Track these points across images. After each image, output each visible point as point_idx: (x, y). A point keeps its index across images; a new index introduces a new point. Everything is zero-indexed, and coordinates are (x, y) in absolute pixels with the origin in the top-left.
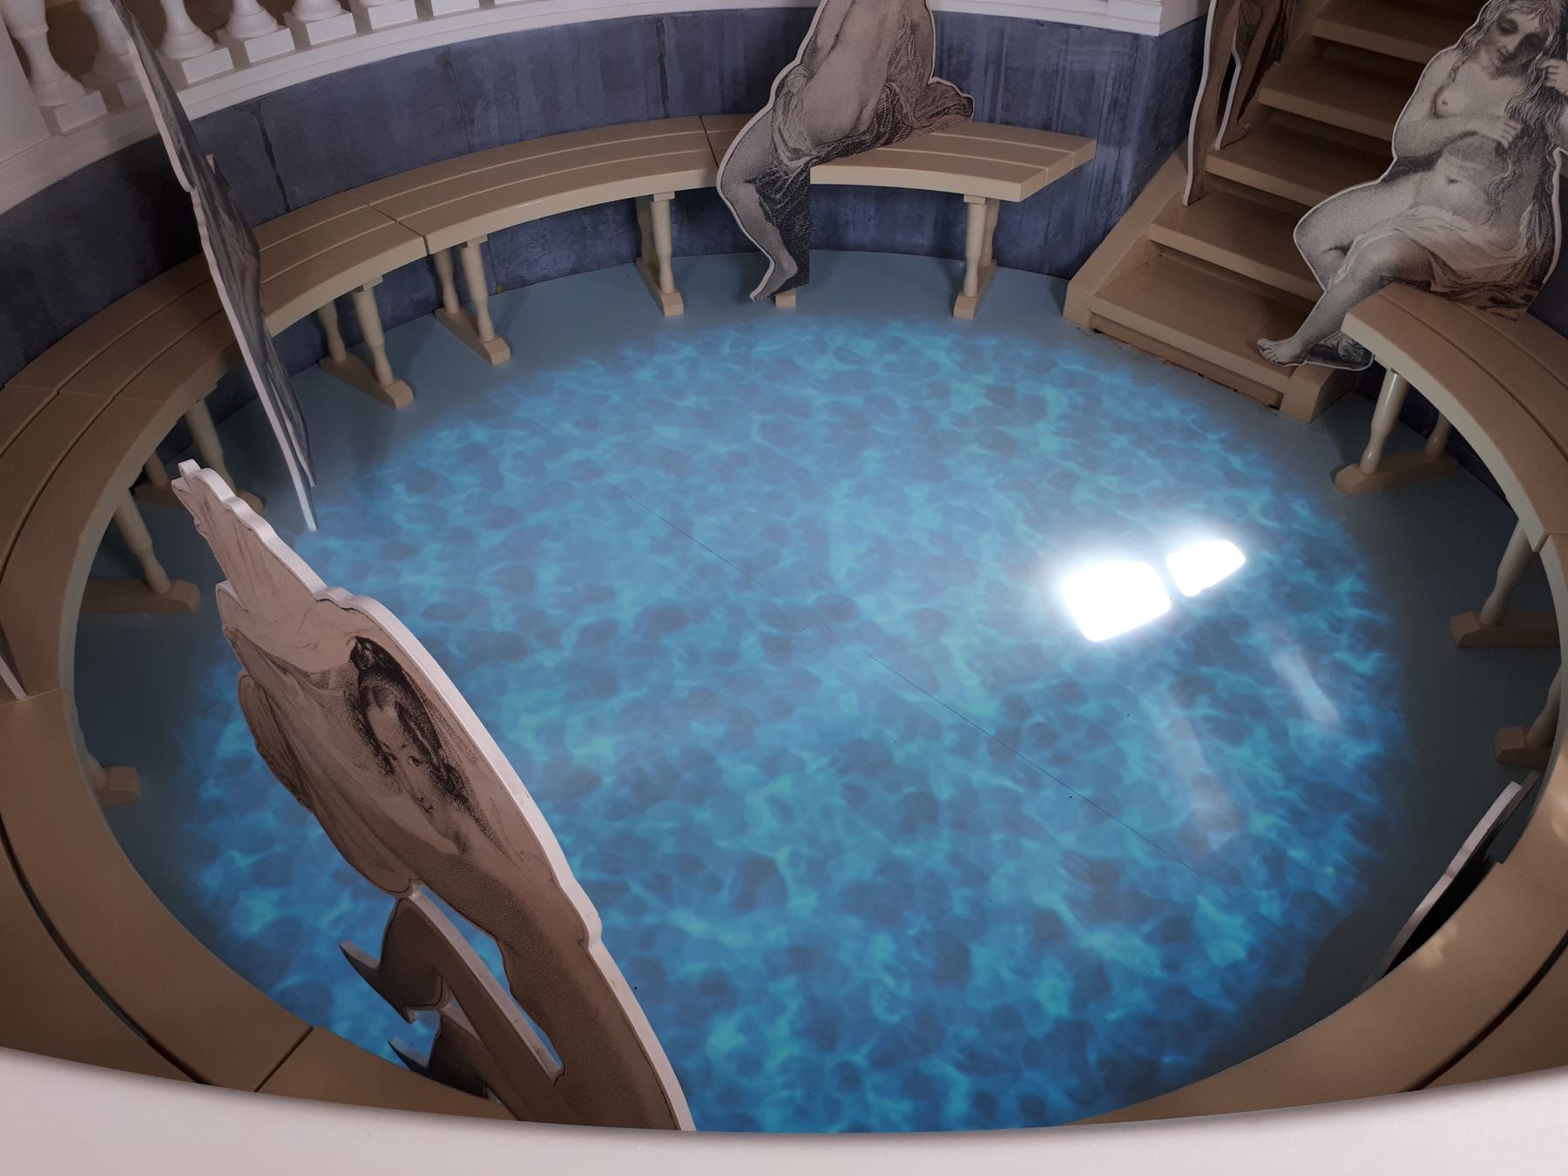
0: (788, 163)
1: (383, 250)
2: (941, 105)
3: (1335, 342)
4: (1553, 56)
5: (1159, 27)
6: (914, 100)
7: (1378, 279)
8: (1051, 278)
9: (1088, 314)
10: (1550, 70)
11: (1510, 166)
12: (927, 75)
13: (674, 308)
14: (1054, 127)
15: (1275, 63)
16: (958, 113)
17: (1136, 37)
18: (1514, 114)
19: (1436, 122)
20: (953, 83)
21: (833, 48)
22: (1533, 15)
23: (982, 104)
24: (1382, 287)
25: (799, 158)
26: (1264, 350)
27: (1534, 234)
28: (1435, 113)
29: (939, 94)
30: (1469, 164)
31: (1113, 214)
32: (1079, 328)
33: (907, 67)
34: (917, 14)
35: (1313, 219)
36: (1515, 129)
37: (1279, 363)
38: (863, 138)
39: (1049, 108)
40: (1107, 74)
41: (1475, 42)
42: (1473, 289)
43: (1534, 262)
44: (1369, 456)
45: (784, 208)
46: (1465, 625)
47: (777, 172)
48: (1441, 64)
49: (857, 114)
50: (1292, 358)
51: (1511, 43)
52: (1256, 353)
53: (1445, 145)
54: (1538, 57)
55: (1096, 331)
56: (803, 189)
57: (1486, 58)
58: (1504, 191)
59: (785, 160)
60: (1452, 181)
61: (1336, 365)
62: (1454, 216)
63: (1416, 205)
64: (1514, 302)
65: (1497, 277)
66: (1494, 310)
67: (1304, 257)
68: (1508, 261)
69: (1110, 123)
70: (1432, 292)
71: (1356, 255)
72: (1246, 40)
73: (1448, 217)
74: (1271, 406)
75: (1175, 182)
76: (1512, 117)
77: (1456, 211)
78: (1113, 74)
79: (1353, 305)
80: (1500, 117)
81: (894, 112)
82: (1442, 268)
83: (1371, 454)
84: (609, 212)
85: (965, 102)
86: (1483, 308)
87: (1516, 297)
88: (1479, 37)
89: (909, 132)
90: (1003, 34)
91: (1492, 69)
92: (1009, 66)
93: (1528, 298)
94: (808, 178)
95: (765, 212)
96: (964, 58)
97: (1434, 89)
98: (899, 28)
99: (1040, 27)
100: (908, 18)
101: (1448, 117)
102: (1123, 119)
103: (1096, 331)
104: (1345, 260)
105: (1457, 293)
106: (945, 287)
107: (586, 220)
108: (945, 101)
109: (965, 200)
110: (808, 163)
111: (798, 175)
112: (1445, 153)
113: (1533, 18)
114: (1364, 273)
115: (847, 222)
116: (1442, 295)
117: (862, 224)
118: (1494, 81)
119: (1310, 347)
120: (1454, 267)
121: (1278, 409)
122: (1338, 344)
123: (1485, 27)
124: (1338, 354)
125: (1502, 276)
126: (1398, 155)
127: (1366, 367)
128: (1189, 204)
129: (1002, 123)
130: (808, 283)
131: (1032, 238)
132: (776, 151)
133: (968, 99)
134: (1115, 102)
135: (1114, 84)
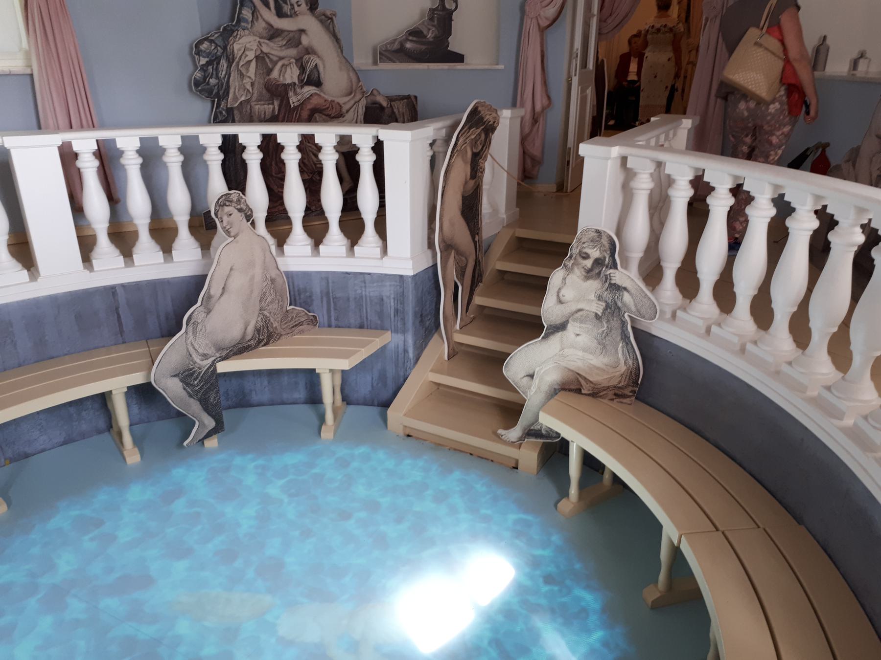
0: (201, 363)
2: (297, 321)
3: (539, 427)
4: (611, 268)
5: (412, 271)
6: (279, 319)
7: (553, 390)
8: (379, 408)
9: (402, 427)
10: (612, 275)
11: (605, 324)
12: (285, 306)
13: (133, 457)
14: (366, 326)
15: (480, 284)
16: (308, 324)
17: (401, 277)
18: (600, 298)
20: (304, 308)
21: (222, 295)
22: (595, 249)
23: (322, 317)
24: (556, 395)
25: (207, 359)
26: (502, 436)
27: (626, 358)
28: (560, 302)
30: (584, 325)
31: (407, 369)
33: (272, 302)
34: (273, 273)
35: (511, 362)
36: (602, 305)
37: (512, 442)
38: (249, 343)
39: (361, 316)
40: (390, 296)
41: (570, 264)
42: (604, 390)
43: (631, 372)
44: (573, 492)
45: (201, 388)
46: (651, 594)
47: (193, 368)
48: (556, 277)
49: (243, 330)
50: (518, 438)
51: (589, 263)
52: (498, 438)
53: (570, 317)
54: (603, 269)
55: (409, 436)
56: (213, 378)
57: (578, 272)
58: (605, 337)
59: (198, 361)
60: (578, 335)
61: (543, 439)
62: (584, 353)
63: (563, 349)
64: (627, 395)
65: (614, 382)
66: (618, 400)
67: (511, 382)
70: (582, 394)
71: (538, 379)
72: (461, 273)
73: (580, 353)
74: (514, 468)
75: (438, 348)
76: (599, 300)
77: (584, 350)
78: (392, 296)
79: (542, 406)
80: (593, 300)
81: (268, 327)
82: (585, 380)
83: (573, 490)
84: (89, 403)
85: (312, 318)
86: (612, 400)
87: (627, 392)
88: (572, 262)
89: (280, 337)
90: (328, 281)
91: (583, 277)
92: (334, 296)
93: (633, 392)
94: (215, 369)
95: (188, 393)
96: (308, 294)
97: (556, 289)
98: (264, 282)
99: (349, 275)
100: (268, 276)
101: (567, 303)
102: (403, 319)
103: (409, 436)
105: (596, 393)
106: (316, 422)
107: (72, 410)
109: (317, 371)
110: (214, 361)
111: (208, 368)
112: (570, 321)
113: (596, 250)
114: (545, 388)
115: (251, 391)
116: (589, 395)
117: (261, 391)
118: (585, 283)
119: (527, 431)
120: (591, 380)
121: (517, 468)
122: (541, 428)
123: (574, 257)
124: (542, 434)
125: (617, 381)
126: (547, 325)
127: (559, 439)
128: (449, 359)
129: (336, 327)
130: (224, 431)
131: (364, 386)
132: (191, 356)
133: (314, 316)
134: (397, 311)
135: (394, 301)
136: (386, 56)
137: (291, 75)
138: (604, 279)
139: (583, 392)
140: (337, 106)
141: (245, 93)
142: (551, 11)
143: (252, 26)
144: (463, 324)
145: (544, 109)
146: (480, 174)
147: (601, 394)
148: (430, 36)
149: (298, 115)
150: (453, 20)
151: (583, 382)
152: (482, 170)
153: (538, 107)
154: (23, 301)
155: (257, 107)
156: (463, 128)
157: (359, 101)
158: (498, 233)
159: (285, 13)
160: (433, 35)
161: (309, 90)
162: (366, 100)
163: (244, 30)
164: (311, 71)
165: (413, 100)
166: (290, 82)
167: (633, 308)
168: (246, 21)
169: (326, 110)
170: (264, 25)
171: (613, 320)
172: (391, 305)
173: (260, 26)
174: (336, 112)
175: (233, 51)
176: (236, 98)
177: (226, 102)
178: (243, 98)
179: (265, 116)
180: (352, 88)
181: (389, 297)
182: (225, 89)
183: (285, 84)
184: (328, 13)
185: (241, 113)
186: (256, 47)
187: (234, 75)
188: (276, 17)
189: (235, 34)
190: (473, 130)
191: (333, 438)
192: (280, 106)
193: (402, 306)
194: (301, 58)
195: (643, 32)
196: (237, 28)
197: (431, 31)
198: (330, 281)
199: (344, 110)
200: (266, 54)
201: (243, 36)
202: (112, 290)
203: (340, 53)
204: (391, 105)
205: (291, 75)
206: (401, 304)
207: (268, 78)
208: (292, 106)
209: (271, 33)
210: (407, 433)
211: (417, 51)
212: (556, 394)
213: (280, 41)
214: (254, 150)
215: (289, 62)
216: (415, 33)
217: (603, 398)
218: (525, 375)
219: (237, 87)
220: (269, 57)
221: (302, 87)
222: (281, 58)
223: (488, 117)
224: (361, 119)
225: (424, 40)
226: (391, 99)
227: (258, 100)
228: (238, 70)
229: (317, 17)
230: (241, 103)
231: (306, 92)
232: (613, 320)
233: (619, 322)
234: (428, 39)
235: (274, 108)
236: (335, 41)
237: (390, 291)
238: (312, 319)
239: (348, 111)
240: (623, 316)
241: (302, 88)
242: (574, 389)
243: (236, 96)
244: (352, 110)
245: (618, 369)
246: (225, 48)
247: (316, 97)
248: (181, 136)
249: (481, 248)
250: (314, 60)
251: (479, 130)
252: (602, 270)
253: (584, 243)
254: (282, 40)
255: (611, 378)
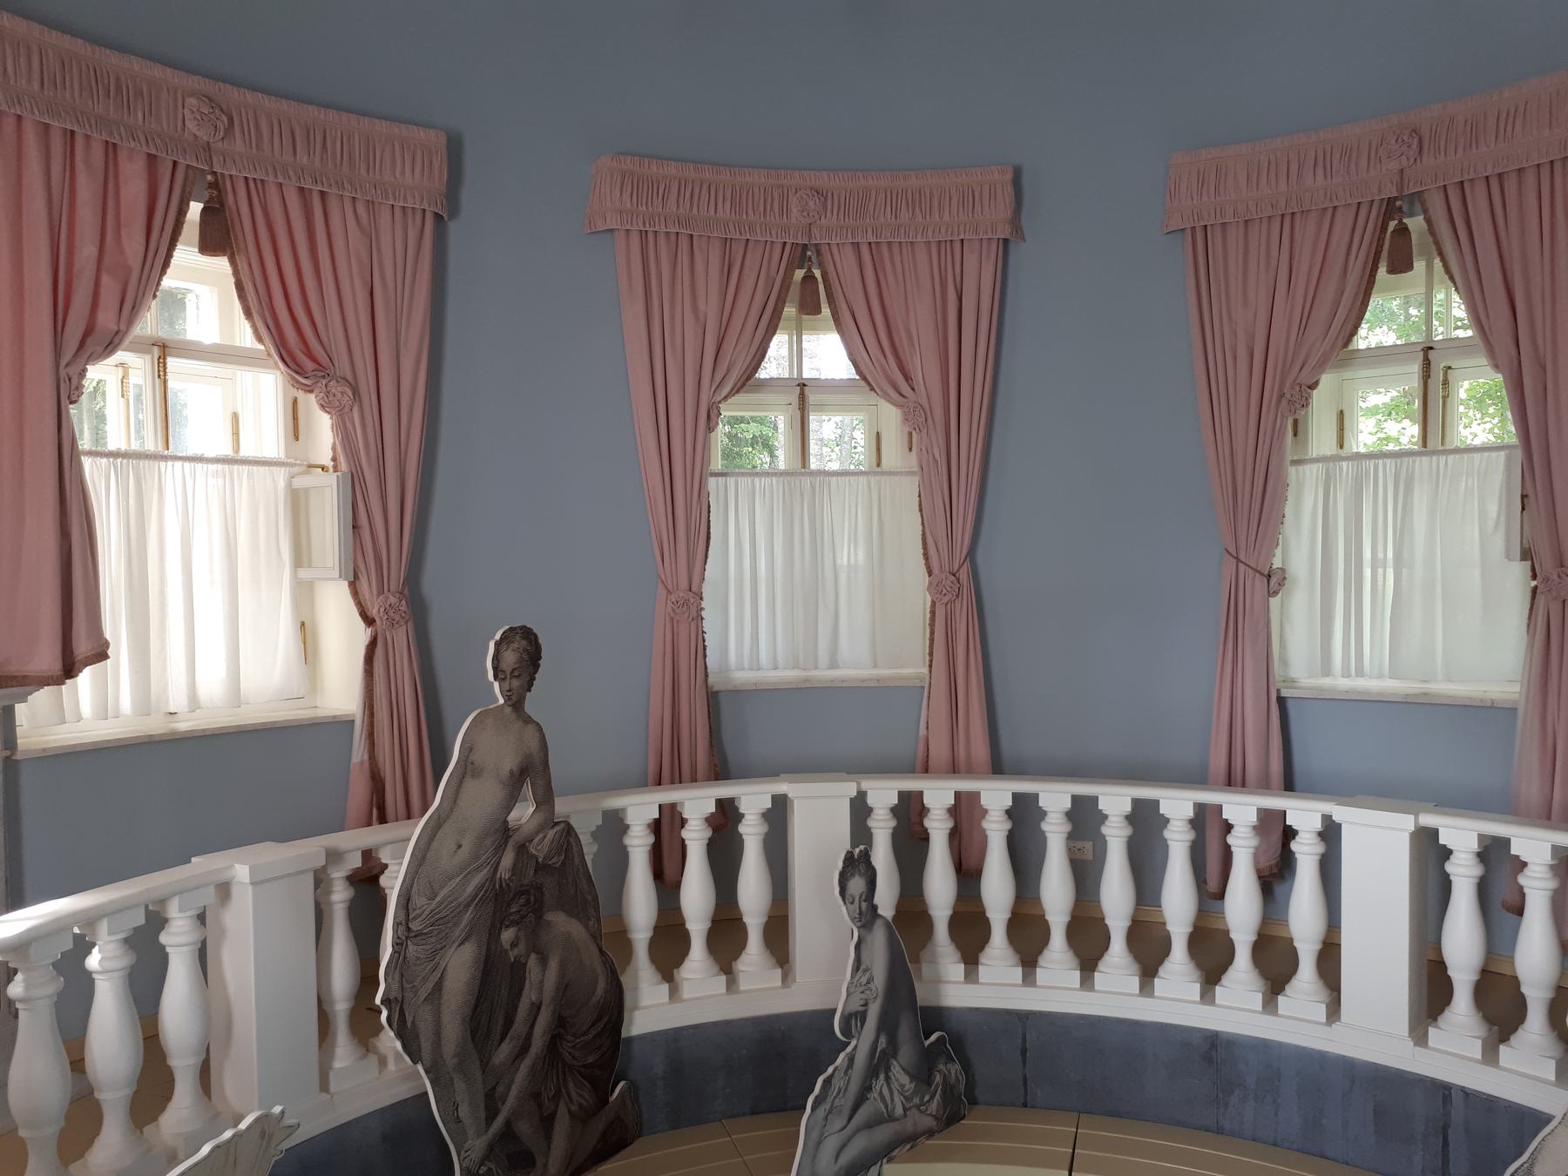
154: (1304, 1049)
202: (1443, 1092)
248: (1013, 793)
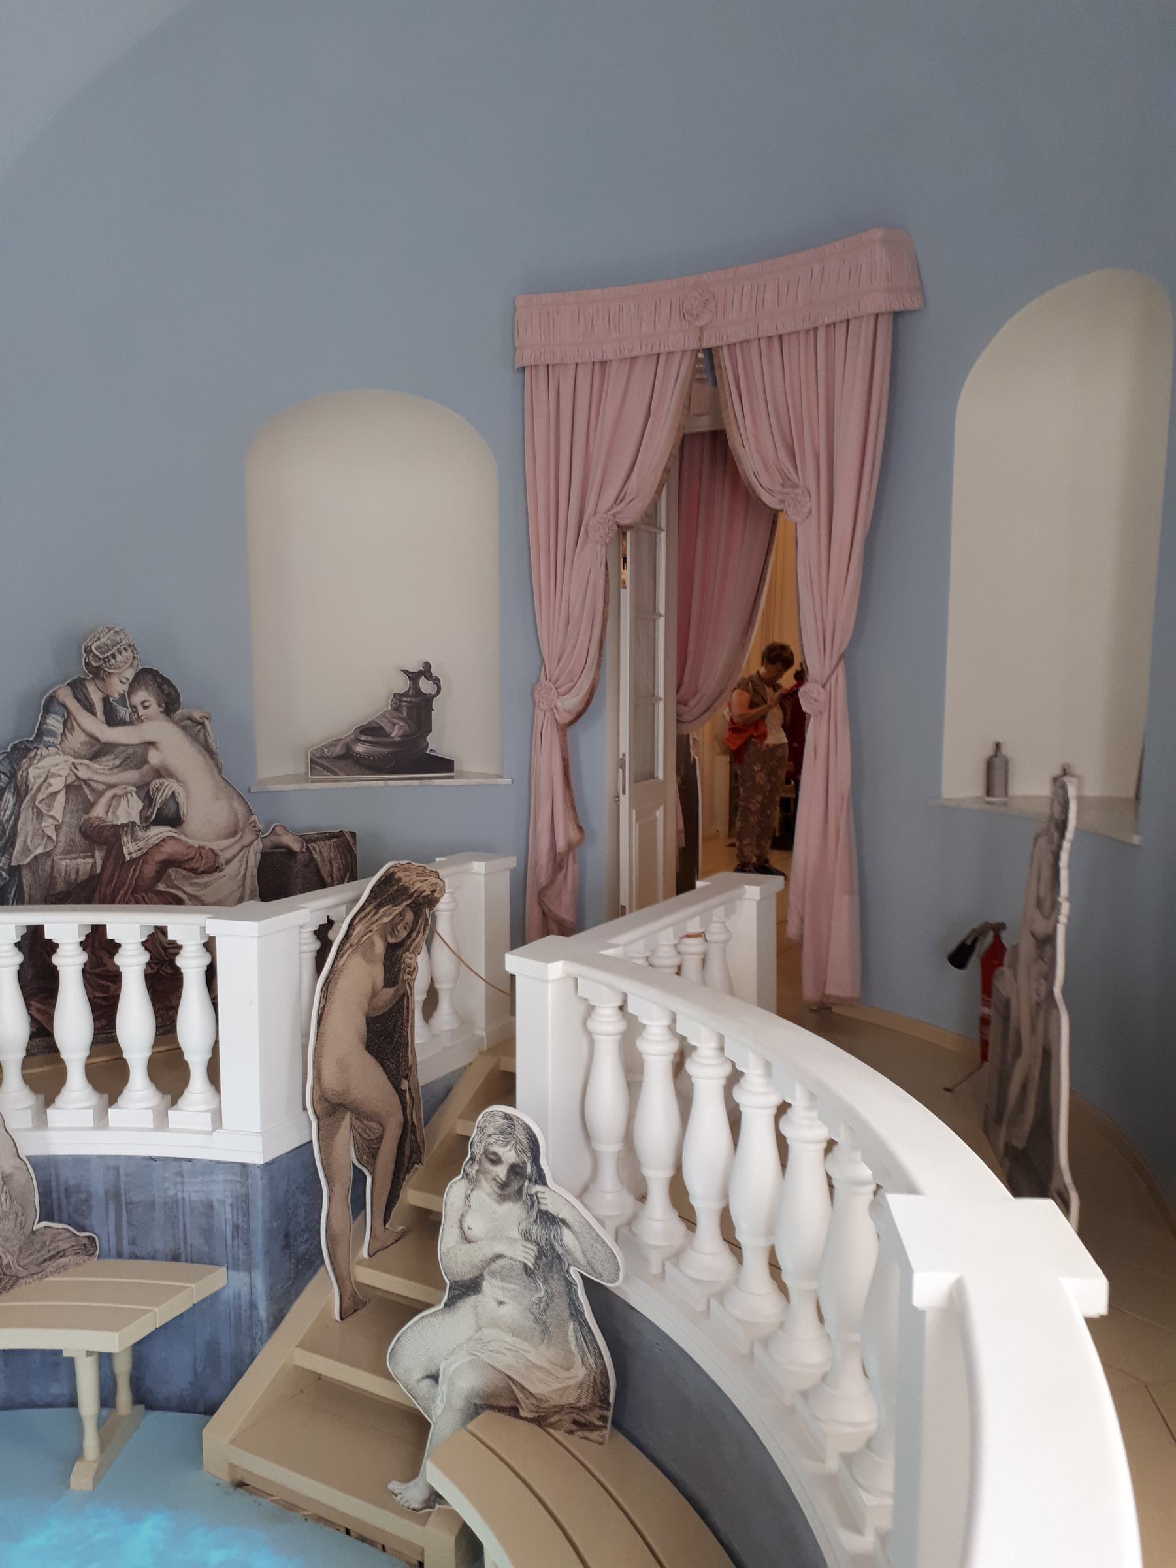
1: (805, 1028)
2: (54, 1249)
4: (536, 1183)
6: (16, 1249)
7: (472, 1408)
10: (540, 1195)
12: (30, 1222)
14: (183, 1257)
16: (76, 1254)
17: (244, 1166)
18: (527, 1236)
19: (468, 1246)
22: (509, 1147)
26: (396, 1495)
27: (584, 1352)
29: (49, 1239)
32: (218, 1485)
37: (413, 1509)
41: (474, 1172)
42: (556, 1413)
51: (501, 1171)
53: (484, 1268)
55: (241, 1485)
58: (545, 1310)
60: (501, 1303)
65: (570, 1399)
66: (580, 1433)
68: (573, 1382)
69: (236, 1249)
72: (369, 1149)
73: (509, 1338)
77: (515, 1332)
78: (229, 1201)
85: (85, 1241)
86: (571, 1432)
87: (593, 1417)
88: (476, 1167)
96: (82, 1196)
97: (457, 1216)
99: (154, 1162)
101: (477, 1241)
102: (247, 1244)
103: (241, 1485)
104: (439, 1389)
108: (59, 1244)
113: (510, 1150)
114: (459, 1403)
120: (532, 1391)
123: (477, 1159)
128: (342, 1319)
133: (89, 1237)
134: (236, 1228)
136: (322, 766)
137: (129, 810)
138: (529, 1202)
139: (523, 1414)
140: (210, 854)
141: (44, 842)
142: (572, 702)
143: (62, 741)
144: (378, 1245)
145: (570, 847)
146: (407, 977)
147: (553, 1420)
148: (396, 733)
149: (137, 873)
150: (433, 710)
151: (520, 1395)
152: (412, 970)
153: (561, 845)
155: (64, 863)
156: (362, 908)
157: (249, 845)
158: (470, 1064)
159: (121, 719)
160: (400, 733)
161: (159, 832)
162: (263, 842)
163: (47, 747)
164: (165, 803)
165: (349, 838)
166: (125, 822)
167: (582, 1261)
168: (52, 734)
169: (190, 862)
170: (83, 738)
171: (553, 1278)
172: (225, 1216)
173: (76, 740)
174: (207, 863)
175: (27, 778)
176: (26, 851)
177: (9, 857)
178: (40, 850)
179: (77, 876)
180: (236, 824)
181: (223, 1203)
182: (10, 837)
183: (117, 825)
184: (197, 715)
185: (34, 873)
186: (68, 771)
187: (26, 814)
188: (105, 727)
189: (32, 754)
190: (387, 910)
191: (91, 1488)
192: (105, 861)
193: (245, 1220)
194: (148, 784)
195: (107, 968)
196: (36, 745)
197: (396, 727)
198: (122, 1172)
199: (222, 860)
200: (84, 781)
201: (46, 757)
203: (217, 775)
204: (308, 849)
205: (129, 810)
206: (244, 1215)
207: (86, 816)
208: (128, 858)
209: (96, 748)
210: (239, 1477)
211: (374, 758)
212: (478, 1414)
213: (109, 761)
214: (8, 952)
215: (124, 791)
216: (371, 730)
217: (555, 1429)
218: (425, 1376)
219: (30, 834)
220: (89, 786)
221: (146, 828)
222: (111, 786)
223: (418, 885)
224: (252, 872)
225: (386, 740)
226: (308, 840)
227: (66, 852)
228: (34, 806)
229: (175, 723)
230: (36, 858)
231: (154, 836)
232: (553, 1278)
233: (563, 1282)
234: (392, 737)
235: (94, 864)
236: (208, 756)
237: (225, 1191)
238: (85, 1245)
239: (228, 862)
240: (568, 1272)
241: (146, 831)
242: (505, 1408)
243: (28, 846)
244: (237, 859)
245: (573, 1372)
246: (12, 776)
247: (171, 843)
249: (416, 1100)
250: (169, 786)
251: (399, 909)
252: (523, 1185)
253: (489, 1136)
254: (114, 759)
255: (564, 1389)
